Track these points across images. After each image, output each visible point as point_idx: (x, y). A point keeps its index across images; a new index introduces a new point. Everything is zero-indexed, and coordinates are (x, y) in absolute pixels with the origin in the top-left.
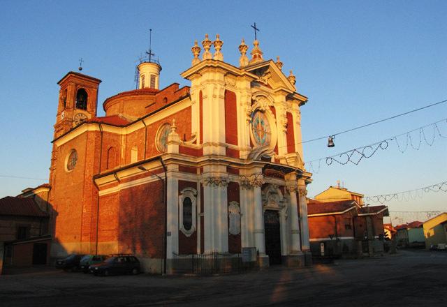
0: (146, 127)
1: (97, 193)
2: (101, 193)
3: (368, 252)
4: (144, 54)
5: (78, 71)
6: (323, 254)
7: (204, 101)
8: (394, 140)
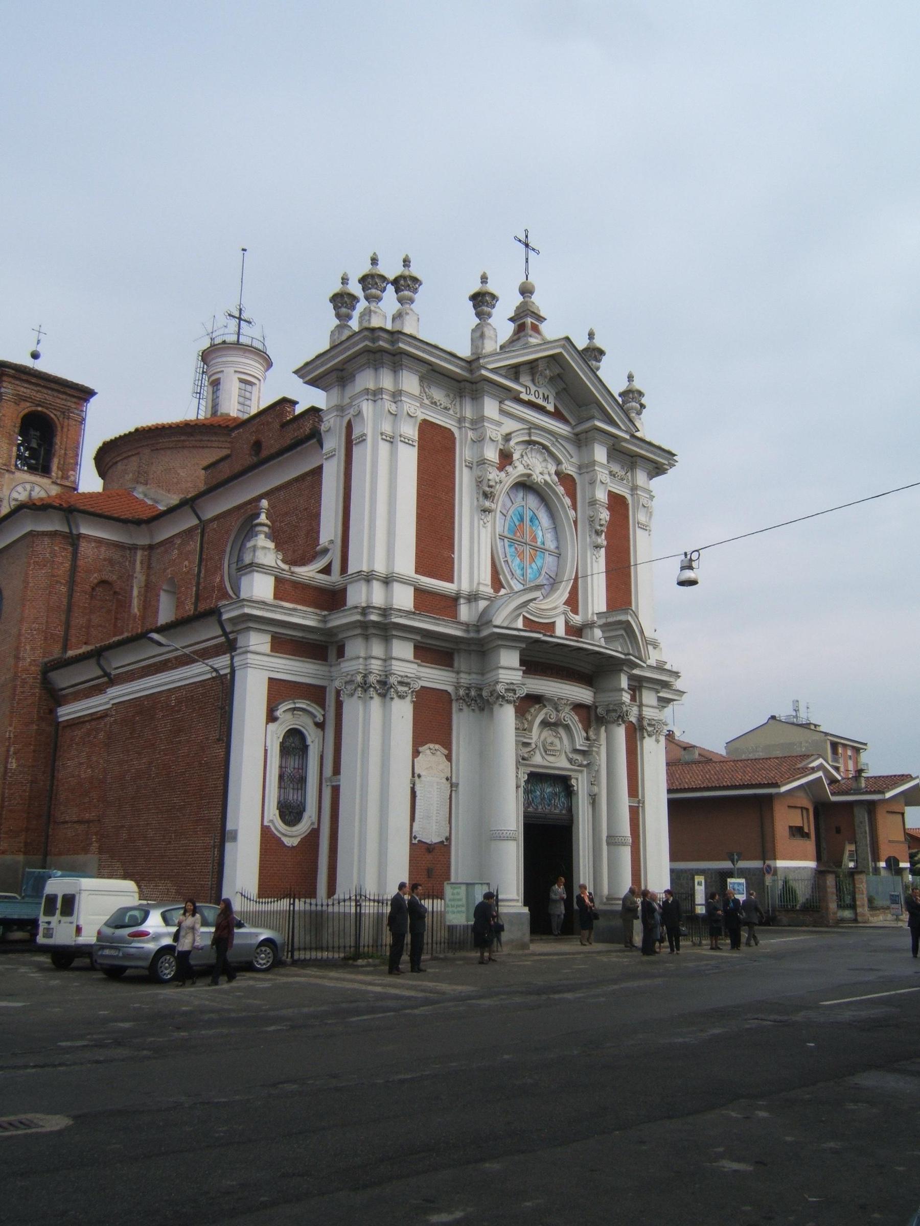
0: (203, 525)
1: (52, 711)
2: (67, 712)
3: (853, 907)
4: (222, 320)
5: (29, 363)
6: (701, 910)
7: (356, 451)
8: (42, 336)
